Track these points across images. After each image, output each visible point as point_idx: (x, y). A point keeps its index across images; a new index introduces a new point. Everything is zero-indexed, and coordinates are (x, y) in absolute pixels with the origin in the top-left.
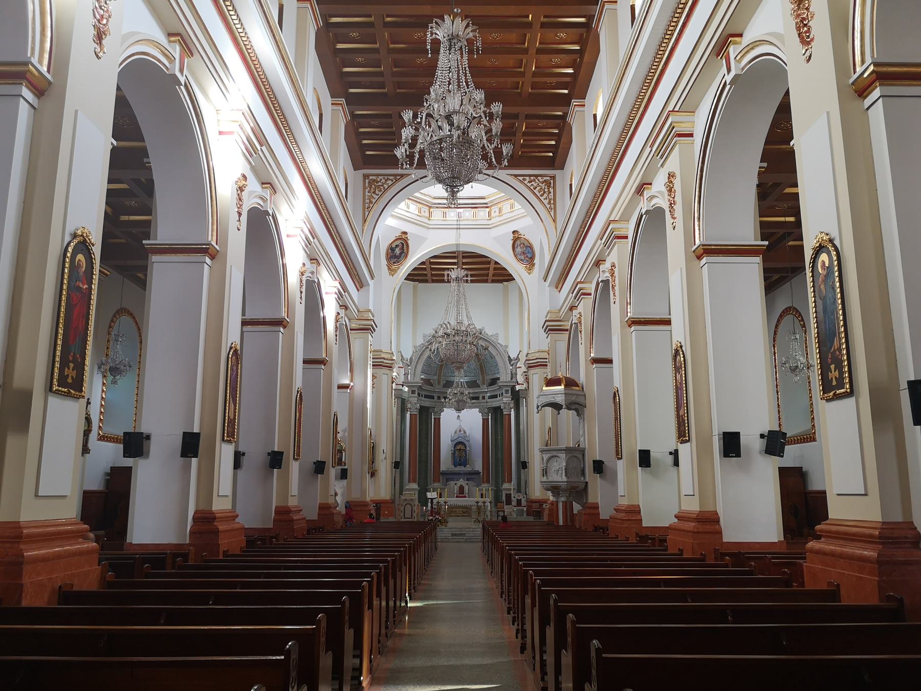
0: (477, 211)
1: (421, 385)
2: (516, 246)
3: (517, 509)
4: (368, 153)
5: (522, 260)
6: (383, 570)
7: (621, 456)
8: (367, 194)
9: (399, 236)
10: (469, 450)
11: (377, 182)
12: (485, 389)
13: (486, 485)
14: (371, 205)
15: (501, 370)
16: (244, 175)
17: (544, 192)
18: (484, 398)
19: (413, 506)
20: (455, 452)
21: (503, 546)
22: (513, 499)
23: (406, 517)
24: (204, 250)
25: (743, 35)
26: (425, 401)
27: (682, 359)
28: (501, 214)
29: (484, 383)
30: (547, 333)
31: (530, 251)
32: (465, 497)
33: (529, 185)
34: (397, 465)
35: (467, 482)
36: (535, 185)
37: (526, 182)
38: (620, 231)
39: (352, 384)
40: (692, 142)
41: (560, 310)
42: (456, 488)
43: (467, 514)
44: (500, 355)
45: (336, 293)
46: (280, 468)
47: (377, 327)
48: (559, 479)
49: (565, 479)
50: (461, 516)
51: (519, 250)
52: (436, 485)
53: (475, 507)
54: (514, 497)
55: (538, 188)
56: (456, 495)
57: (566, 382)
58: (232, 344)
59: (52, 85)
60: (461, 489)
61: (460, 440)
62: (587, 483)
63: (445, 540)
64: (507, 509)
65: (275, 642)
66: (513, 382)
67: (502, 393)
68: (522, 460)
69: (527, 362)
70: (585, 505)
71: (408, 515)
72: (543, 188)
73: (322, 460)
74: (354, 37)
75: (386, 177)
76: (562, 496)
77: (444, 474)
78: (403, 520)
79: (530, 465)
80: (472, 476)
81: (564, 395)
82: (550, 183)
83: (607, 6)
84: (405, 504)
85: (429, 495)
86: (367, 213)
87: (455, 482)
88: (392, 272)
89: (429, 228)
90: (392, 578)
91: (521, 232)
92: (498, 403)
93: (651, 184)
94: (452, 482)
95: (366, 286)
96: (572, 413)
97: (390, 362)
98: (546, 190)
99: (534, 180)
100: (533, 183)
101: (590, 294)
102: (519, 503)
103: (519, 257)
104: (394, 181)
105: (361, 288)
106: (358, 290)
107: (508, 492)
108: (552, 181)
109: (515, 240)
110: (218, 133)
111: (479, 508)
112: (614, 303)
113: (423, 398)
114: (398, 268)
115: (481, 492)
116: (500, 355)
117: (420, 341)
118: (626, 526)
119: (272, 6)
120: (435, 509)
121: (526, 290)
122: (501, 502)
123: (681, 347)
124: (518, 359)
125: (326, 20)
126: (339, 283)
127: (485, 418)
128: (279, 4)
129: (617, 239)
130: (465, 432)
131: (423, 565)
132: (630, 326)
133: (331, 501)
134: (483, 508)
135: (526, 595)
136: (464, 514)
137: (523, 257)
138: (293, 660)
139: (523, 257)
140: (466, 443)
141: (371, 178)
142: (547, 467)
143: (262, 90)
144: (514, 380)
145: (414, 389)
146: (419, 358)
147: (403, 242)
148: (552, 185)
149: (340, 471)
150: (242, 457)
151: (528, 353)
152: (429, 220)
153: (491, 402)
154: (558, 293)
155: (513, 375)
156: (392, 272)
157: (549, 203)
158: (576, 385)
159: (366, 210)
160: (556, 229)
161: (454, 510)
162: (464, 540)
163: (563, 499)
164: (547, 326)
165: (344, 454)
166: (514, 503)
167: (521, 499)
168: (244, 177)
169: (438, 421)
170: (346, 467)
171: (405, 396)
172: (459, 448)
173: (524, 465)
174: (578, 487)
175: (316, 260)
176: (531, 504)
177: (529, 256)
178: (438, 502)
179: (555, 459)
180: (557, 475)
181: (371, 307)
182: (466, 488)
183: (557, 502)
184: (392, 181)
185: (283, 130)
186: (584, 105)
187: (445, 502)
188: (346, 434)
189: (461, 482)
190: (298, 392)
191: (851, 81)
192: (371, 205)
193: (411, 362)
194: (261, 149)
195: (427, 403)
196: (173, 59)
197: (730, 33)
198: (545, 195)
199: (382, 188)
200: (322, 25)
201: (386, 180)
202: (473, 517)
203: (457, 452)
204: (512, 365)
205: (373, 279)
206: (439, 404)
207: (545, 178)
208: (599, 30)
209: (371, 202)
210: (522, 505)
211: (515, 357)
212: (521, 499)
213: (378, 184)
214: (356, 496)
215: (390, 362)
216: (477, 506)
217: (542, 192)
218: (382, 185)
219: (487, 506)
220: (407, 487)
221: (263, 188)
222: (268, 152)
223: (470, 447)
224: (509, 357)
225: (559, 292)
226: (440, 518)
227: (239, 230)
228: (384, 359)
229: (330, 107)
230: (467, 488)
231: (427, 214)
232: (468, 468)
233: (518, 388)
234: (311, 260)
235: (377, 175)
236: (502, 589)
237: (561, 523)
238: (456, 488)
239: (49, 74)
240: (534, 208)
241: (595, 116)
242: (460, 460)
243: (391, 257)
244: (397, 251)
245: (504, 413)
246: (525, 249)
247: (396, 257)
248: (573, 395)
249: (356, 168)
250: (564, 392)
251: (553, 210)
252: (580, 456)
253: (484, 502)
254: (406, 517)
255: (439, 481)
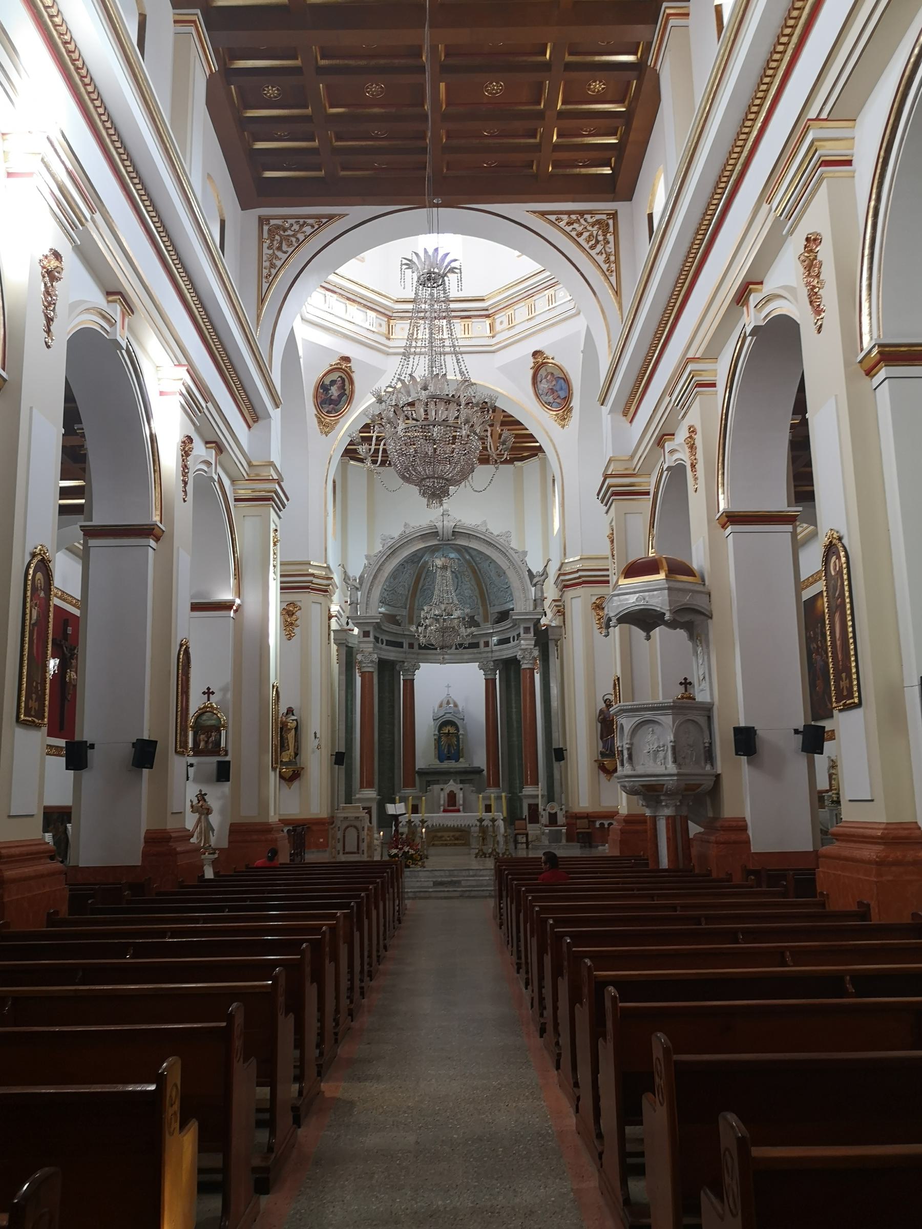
0: (470, 323)
1: (379, 621)
2: (539, 379)
3: (550, 830)
4: (268, 174)
5: (549, 404)
6: (380, 884)
7: (860, 697)
8: (266, 251)
9: (337, 364)
10: (462, 734)
11: (285, 230)
12: (489, 628)
13: (493, 790)
14: (274, 271)
15: (517, 594)
16: (56, 251)
17: (597, 242)
18: (487, 644)
19: (360, 829)
20: (440, 738)
21: (519, 891)
22: (543, 813)
23: (347, 850)
24: (148, 531)
25: (764, 283)
26: (385, 650)
27: (843, 559)
28: (511, 325)
29: (486, 620)
30: (606, 505)
31: (564, 386)
32: (458, 811)
33: (568, 229)
34: (339, 758)
35: (461, 786)
36: (580, 229)
37: (562, 224)
38: (700, 375)
39: (238, 601)
40: (851, 174)
41: (632, 457)
42: (442, 796)
43: (463, 842)
44: (515, 568)
45: (182, 394)
46: (151, 768)
47: (288, 500)
48: (660, 770)
49: (672, 768)
50: (451, 845)
51: (544, 386)
52: (409, 791)
53: (477, 829)
54: (544, 810)
55: (586, 234)
56: (442, 808)
57: (668, 567)
58: (182, 641)
59: (6, 383)
60: (452, 797)
61: (448, 717)
62: (718, 776)
63: (422, 894)
64: (533, 830)
65: (265, 970)
66: (538, 613)
67: (519, 635)
68: (555, 746)
69: (562, 578)
70: (713, 824)
71: (351, 845)
72: (595, 235)
73: (152, 739)
74: (270, 97)
75: (302, 221)
76: (666, 806)
77: (423, 773)
78: (343, 858)
79: (570, 754)
80: (469, 775)
81: (666, 591)
82: (608, 225)
83: (672, 22)
84: (343, 827)
85: (391, 809)
86: (265, 286)
87: (442, 786)
88: (326, 428)
89: (388, 354)
90: (344, 943)
91: (548, 353)
92: (511, 651)
93: (761, 283)
94: (435, 786)
95: (265, 418)
96: (681, 634)
97: (325, 582)
98: (601, 238)
99: (578, 221)
100: (576, 225)
101: (648, 493)
102: (553, 818)
103: (544, 398)
104: (316, 227)
105: (255, 422)
106: (249, 427)
107: (532, 801)
108: (611, 222)
109: (537, 368)
110: (6, 175)
111: (483, 830)
112: (696, 491)
113: (384, 646)
114: (337, 422)
115: (488, 803)
116: (515, 568)
117: (378, 548)
118: (890, 878)
119: (127, 21)
120: (402, 834)
121: (558, 455)
122: (522, 819)
123: (840, 539)
124: (545, 574)
125: (225, 64)
126: (188, 371)
127: (489, 677)
128: (140, 14)
129: (699, 387)
130: (456, 705)
131: (391, 922)
132: (724, 527)
133: (171, 825)
134: (491, 829)
135: (545, 955)
136: (456, 842)
137: (550, 399)
138: (238, 1025)
139: (550, 399)
140: (459, 723)
141: (272, 222)
142: (632, 744)
143: (218, 360)
144: (539, 609)
145: (367, 629)
146: (375, 577)
147: (344, 376)
148: (611, 229)
149: (215, 766)
150: (90, 751)
151: (562, 564)
152: (389, 339)
153: (500, 650)
154: (629, 424)
155: (539, 601)
156: (326, 428)
157: (607, 261)
158: (689, 572)
159: (264, 280)
160: (621, 308)
161: (439, 834)
162: (457, 894)
163: (668, 812)
164: (609, 487)
165: (223, 733)
166: (544, 819)
167: (556, 812)
168: (57, 255)
169: (410, 684)
170: (227, 759)
171: (353, 642)
172: (447, 731)
173: (559, 754)
174: (701, 785)
175: (120, 293)
176: (574, 821)
177: (562, 394)
178: (410, 822)
179: (649, 728)
180: (655, 760)
181: (275, 458)
182: (460, 796)
183: (654, 819)
184: (313, 227)
185: (131, 185)
186: (688, 15)
187: (423, 822)
188: (229, 695)
189: (452, 786)
190: (181, 645)
191: (717, 517)
192: (274, 271)
193: (361, 583)
194: (206, 406)
195: (391, 654)
196: (114, 321)
197: (749, 281)
198: (599, 247)
199: (294, 239)
200: (217, 69)
201: (302, 226)
202: (473, 847)
203: (443, 738)
204: (535, 585)
205: (277, 407)
206: (413, 656)
207: (598, 217)
208: (658, 68)
209: (273, 266)
210: (559, 824)
211: (541, 569)
212: (556, 812)
213: (286, 233)
214: (248, 813)
215: (325, 582)
216: (481, 826)
217: (593, 242)
218: (293, 236)
219: (498, 826)
220: (358, 796)
221: (207, 448)
222: (217, 412)
223: (465, 728)
224: (529, 571)
225: (631, 422)
226: (412, 852)
227: (48, 347)
228: (313, 575)
229: (170, 27)
230: (461, 795)
231: (384, 329)
232: (462, 764)
233: (544, 621)
234: (207, 443)
235: (285, 218)
236: (500, 919)
237: (664, 863)
238: (443, 798)
239: (4, 371)
240: (578, 270)
241: (650, 217)
242: (449, 751)
243: (323, 402)
244: (334, 391)
245: (524, 666)
246: (554, 383)
247: (331, 401)
248: (685, 591)
249: (245, 205)
250: (667, 586)
251: (614, 274)
252: (702, 721)
253: (493, 820)
254: (347, 850)
255: (414, 786)
